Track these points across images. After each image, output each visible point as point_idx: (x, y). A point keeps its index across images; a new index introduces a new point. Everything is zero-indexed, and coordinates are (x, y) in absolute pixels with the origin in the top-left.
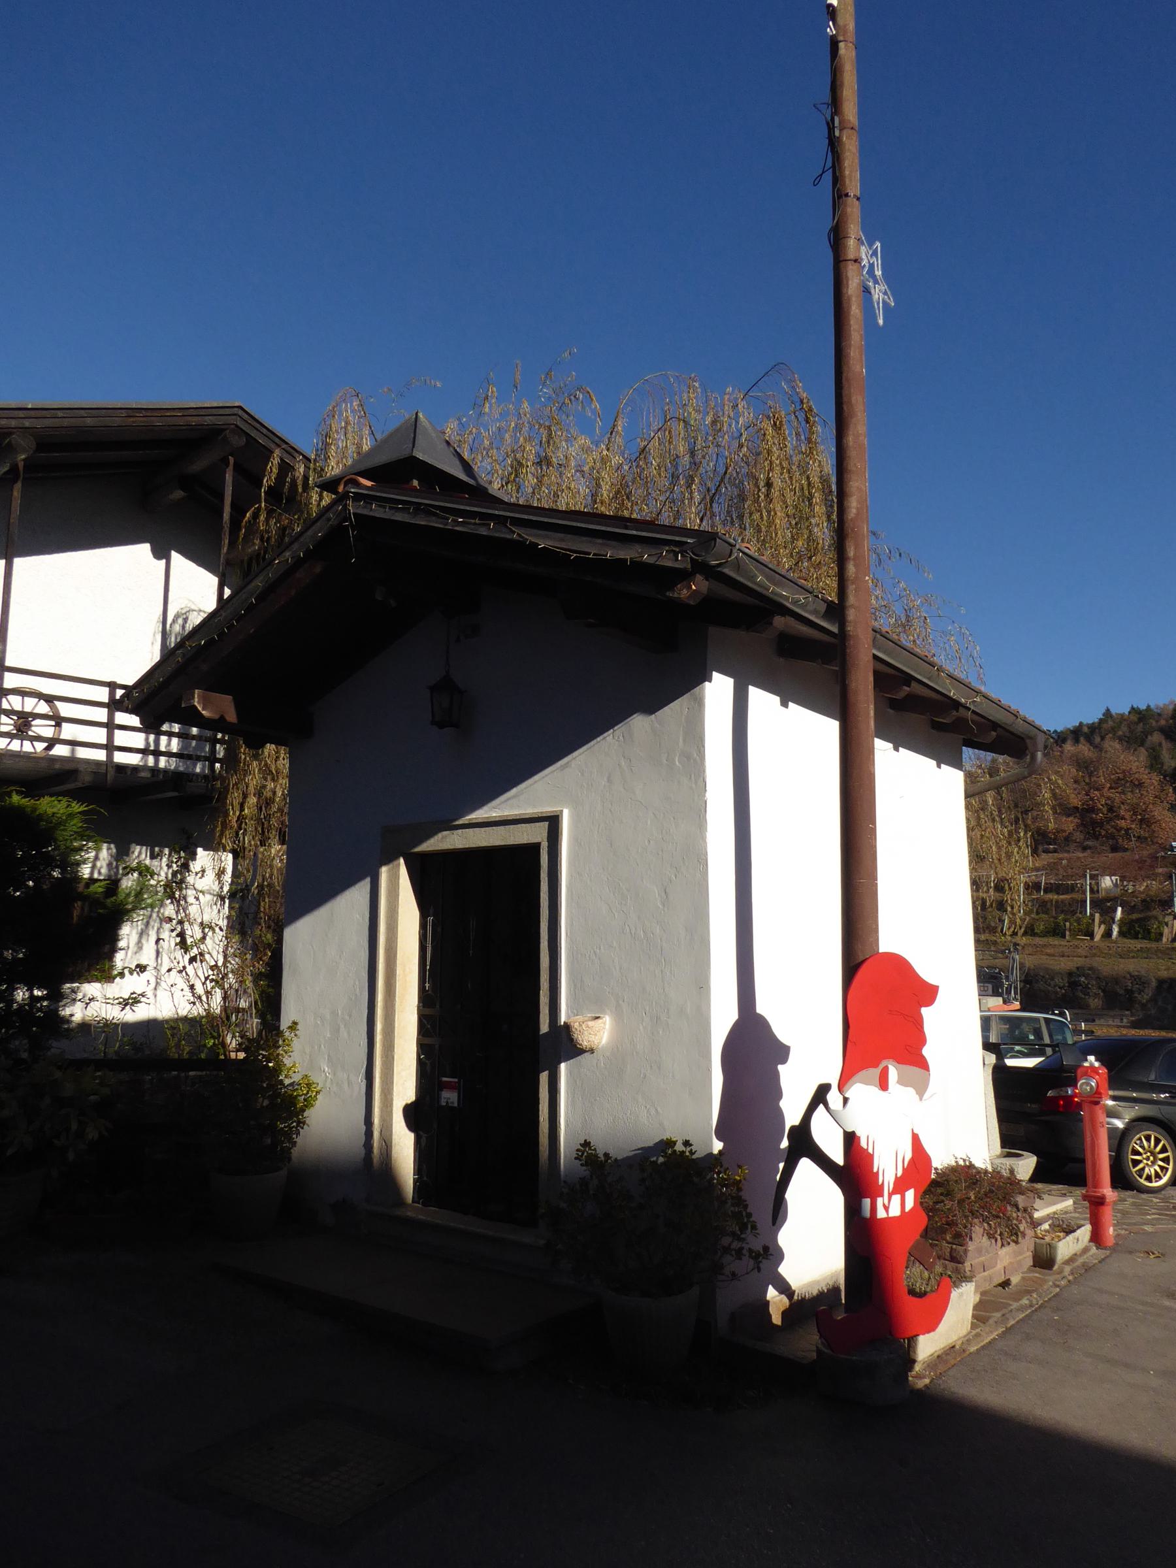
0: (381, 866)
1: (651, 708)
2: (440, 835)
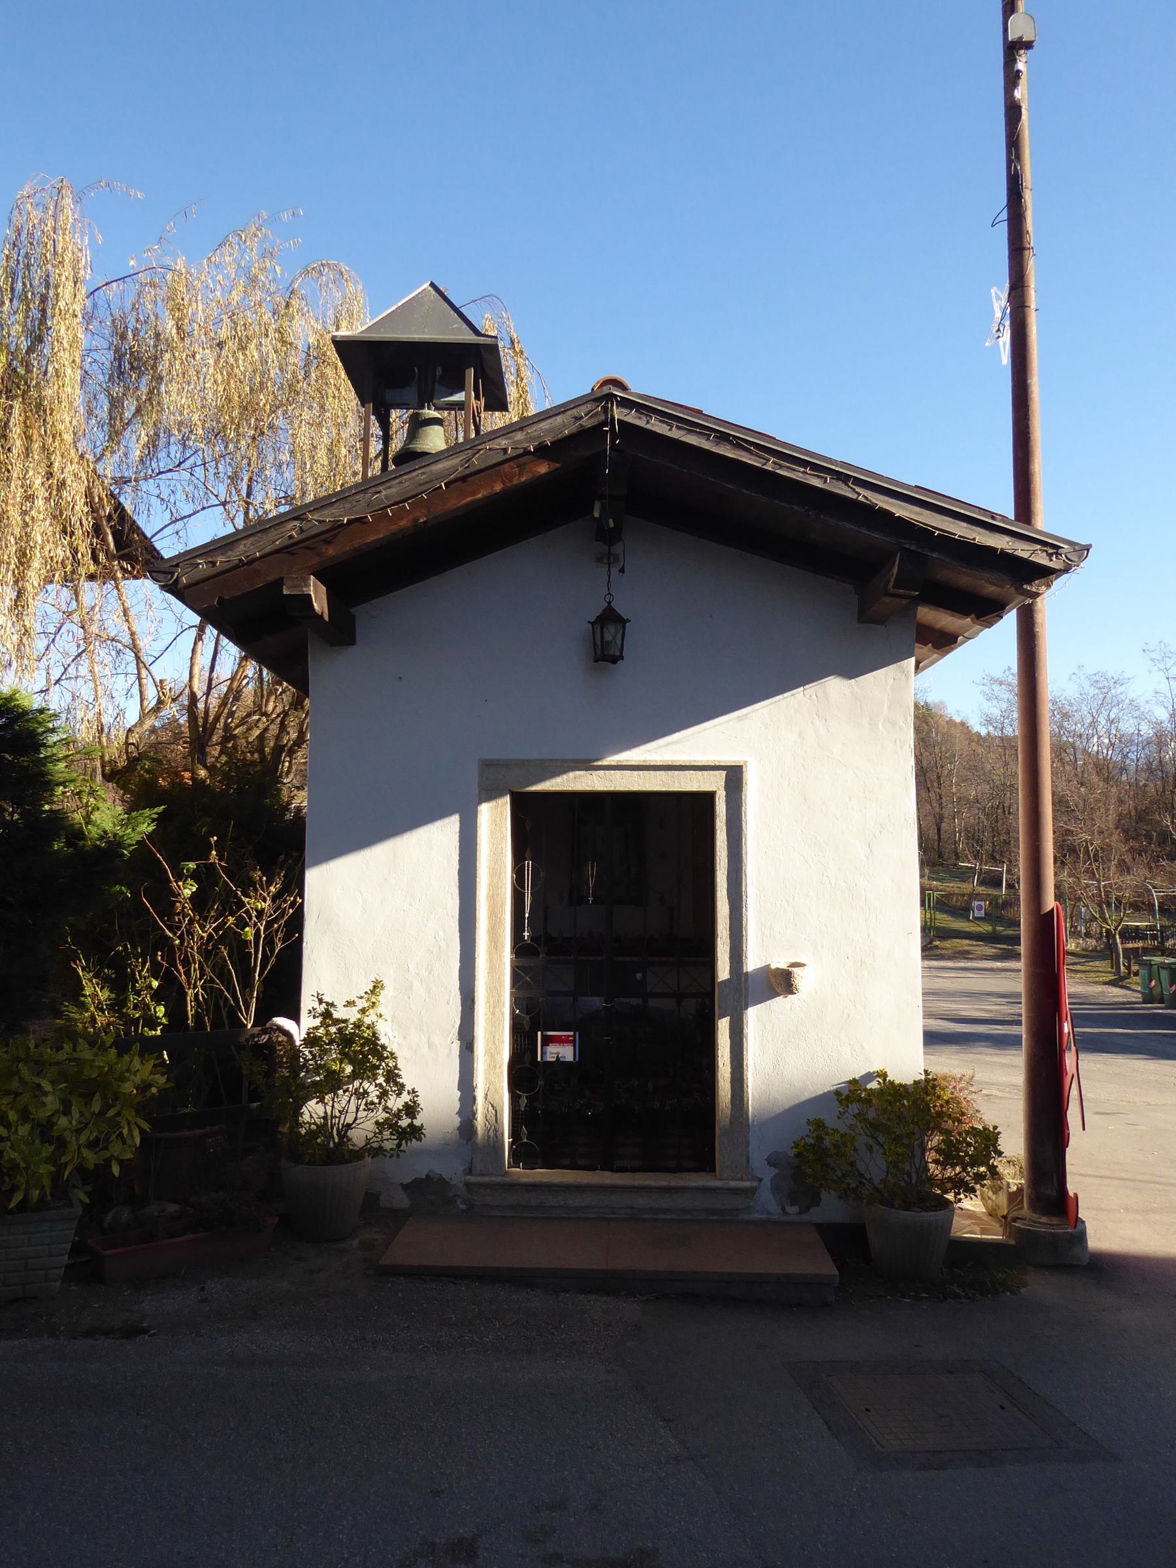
0: (480, 803)
1: (851, 671)
2: (571, 775)
